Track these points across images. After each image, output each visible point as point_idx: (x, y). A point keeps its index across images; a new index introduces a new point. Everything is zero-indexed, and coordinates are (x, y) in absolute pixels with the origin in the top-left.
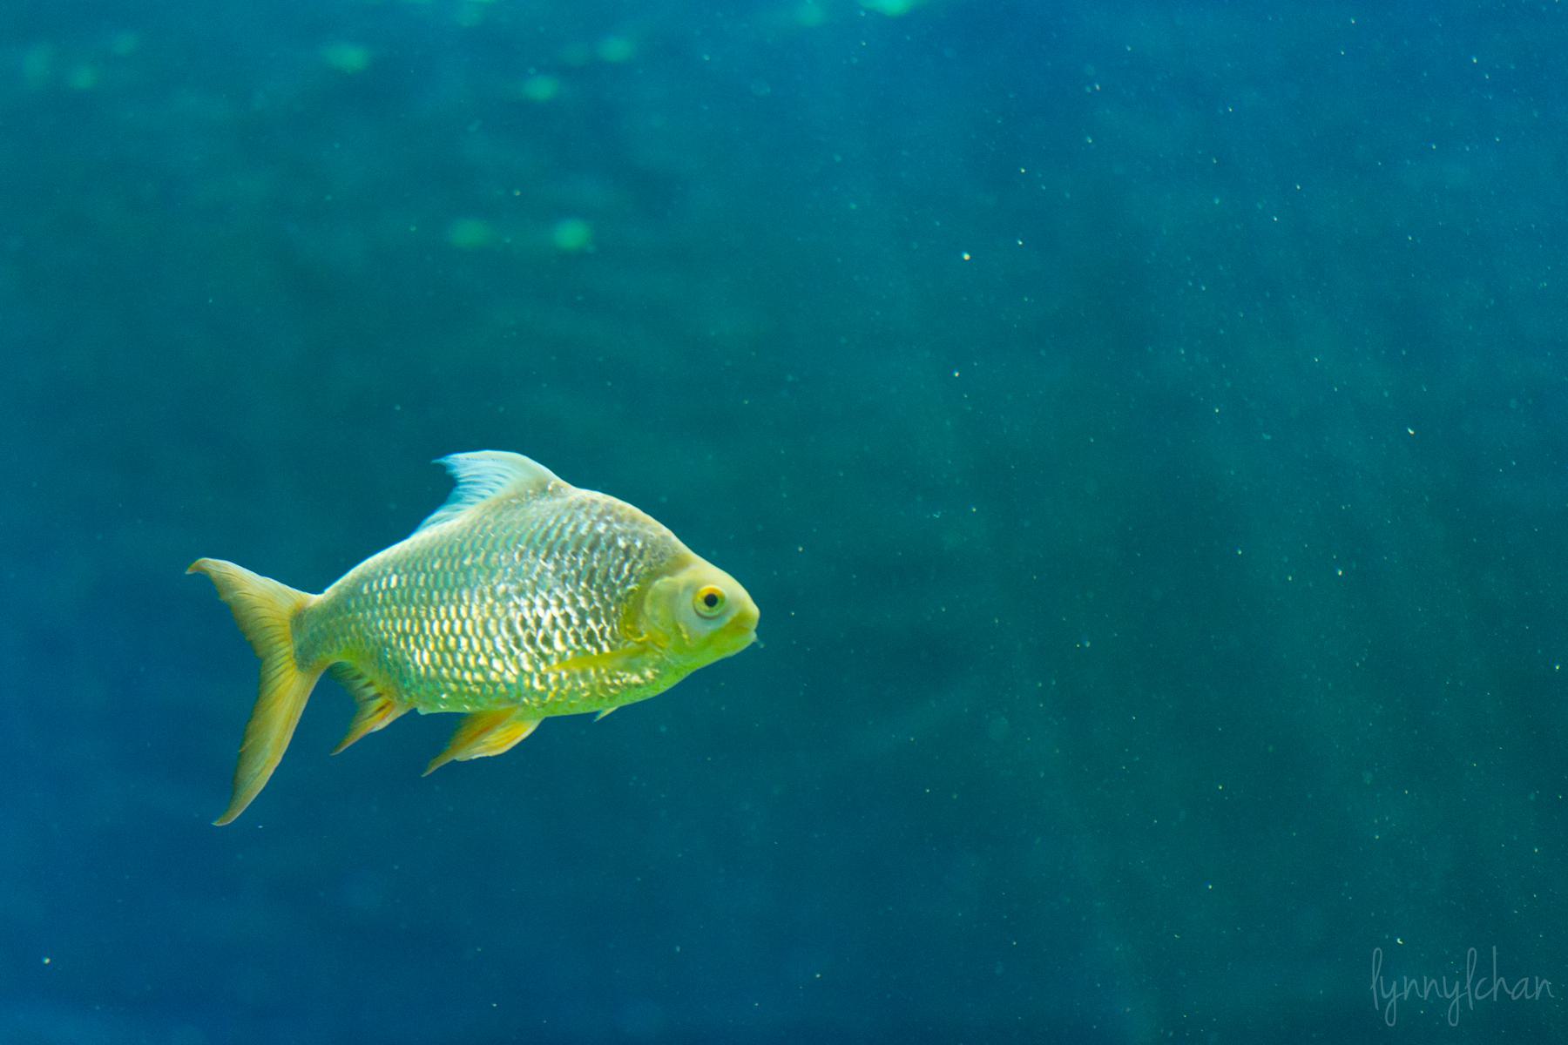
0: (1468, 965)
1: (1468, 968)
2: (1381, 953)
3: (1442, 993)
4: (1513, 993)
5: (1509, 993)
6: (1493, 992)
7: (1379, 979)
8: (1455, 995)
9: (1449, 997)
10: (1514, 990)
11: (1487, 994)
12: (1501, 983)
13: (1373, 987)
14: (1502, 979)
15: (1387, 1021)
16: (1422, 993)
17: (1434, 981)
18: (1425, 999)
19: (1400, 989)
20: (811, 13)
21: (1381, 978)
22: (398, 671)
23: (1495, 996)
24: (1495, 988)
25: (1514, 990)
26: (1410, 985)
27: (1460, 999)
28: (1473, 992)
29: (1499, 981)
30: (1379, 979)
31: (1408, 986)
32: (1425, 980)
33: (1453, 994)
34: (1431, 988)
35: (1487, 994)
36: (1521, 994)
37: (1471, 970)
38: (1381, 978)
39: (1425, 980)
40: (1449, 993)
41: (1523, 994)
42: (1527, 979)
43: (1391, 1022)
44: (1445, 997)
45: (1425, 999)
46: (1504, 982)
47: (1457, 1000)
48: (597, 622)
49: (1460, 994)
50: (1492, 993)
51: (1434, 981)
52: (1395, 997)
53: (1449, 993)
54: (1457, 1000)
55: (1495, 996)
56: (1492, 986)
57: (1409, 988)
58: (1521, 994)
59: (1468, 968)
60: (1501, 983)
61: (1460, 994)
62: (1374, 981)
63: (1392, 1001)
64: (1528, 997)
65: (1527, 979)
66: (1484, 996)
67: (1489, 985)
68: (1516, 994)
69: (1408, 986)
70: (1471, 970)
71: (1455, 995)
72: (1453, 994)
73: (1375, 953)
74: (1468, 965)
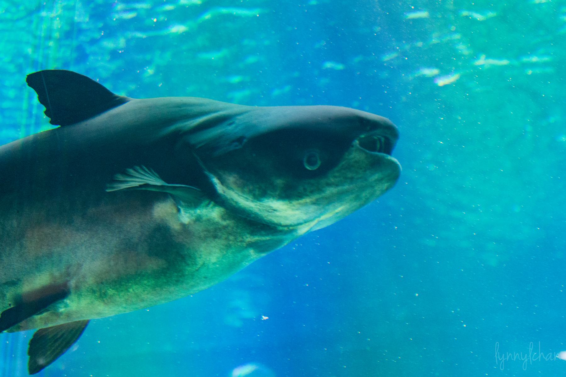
0: (496, 349)
1: (496, 350)
2: (533, 344)
3: (520, 358)
4: (546, 358)
5: (545, 358)
6: (539, 358)
7: (498, 353)
8: (525, 359)
9: (523, 359)
10: (547, 357)
11: (537, 359)
12: (542, 355)
13: (496, 356)
14: (542, 353)
15: (523, 368)
16: (513, 358)
17: (510, 354)
18: (515, 360)
19: (505, 357)
20: (313, 3)
21: (499, 353)
22: (387, 55)
23: (540, 359)
24: (540, 357)
25: (547, 357)
26: (509, 355)
27: (504, 361)
28: (532, 358)
29: (541, 354)
30: (498, 353)
31: (508, 355)
32: (507, 354)
33: (502, 358)
34: (509, 357)
35: (537, 359)
36: (549, 358)
37: (497, 350)
38: (499, 353)
39: (507, 354)
40: (501, 358)
41: (550, 358)
42: (551, 353)
43: (525, 369)
44: (521, 360)
45: (515, 360)
46: (543, 354)
47: (503, 361)
48: (413, 109)
49: (527, 359)
50: (539, 359)
51: (510, 354)
52: (526, 360)
53: (523, 358)
54: (503, 361)
55: (540, 359)
56: (539, 356)
57: (509, 356)
58: (549, 358)
59: (496, 350)
60: (542, 355)
61: (527, 359)
62: (496, 354)
63: (502, 361)
64: (551, 360)
65: (551, 353)
66: (536, 359)
67: (538, 355)
68: (547, 358)
69: (508, 355)
70: (497, 350)
71: (525, 359)
72: (502, 358)
73: (496, 343)
74: (496, 349)
